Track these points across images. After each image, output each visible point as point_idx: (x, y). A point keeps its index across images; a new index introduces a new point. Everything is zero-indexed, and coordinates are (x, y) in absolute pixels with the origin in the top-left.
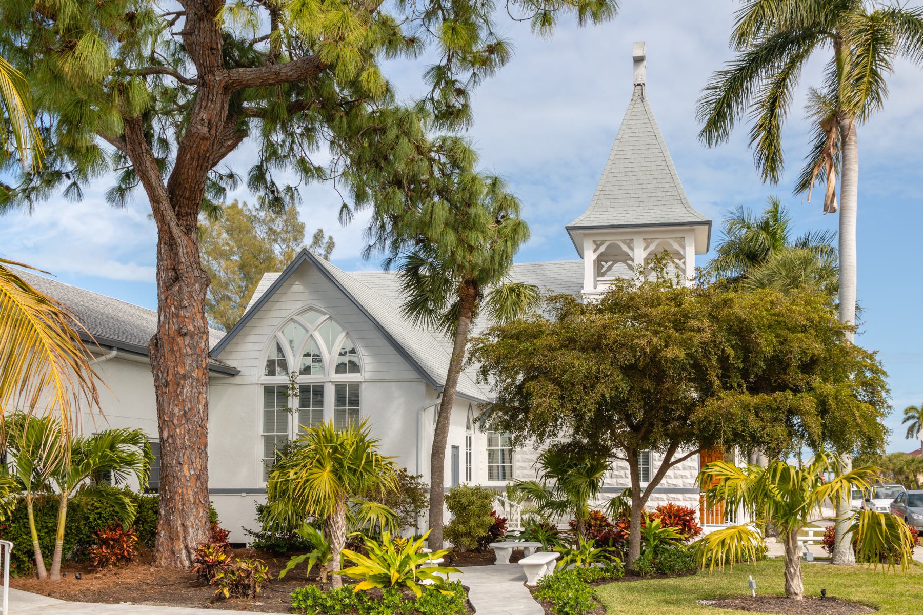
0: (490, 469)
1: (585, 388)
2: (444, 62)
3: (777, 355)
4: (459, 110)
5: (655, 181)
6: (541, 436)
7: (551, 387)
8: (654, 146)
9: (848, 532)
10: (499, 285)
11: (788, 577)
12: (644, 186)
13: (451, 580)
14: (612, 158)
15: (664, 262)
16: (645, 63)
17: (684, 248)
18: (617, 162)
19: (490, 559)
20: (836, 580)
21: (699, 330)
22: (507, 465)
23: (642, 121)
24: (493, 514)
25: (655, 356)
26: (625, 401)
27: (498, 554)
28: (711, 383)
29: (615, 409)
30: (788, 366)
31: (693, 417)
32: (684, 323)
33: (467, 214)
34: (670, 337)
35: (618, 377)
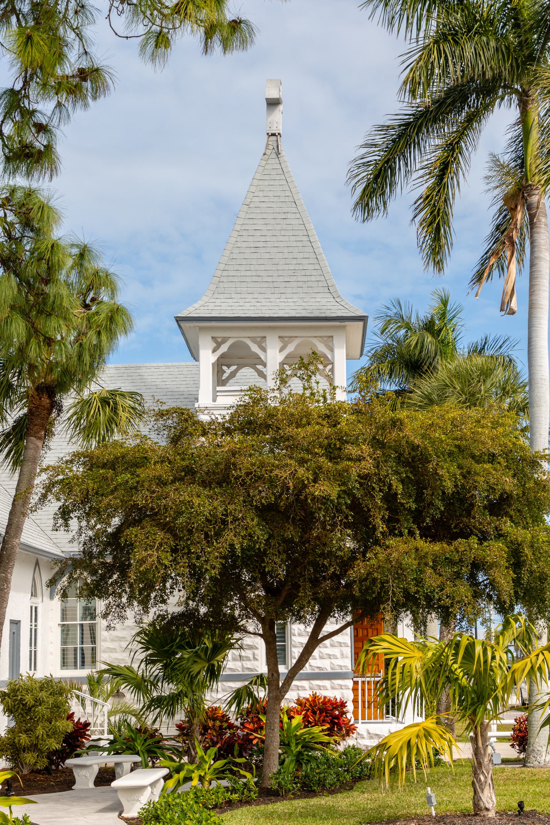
0: (64, 652)
1: (207, 536)
2: (18, 86)
3: (458, 493)
4: (40, 152)
5: (294, 261)
6: (145, 603)
7: (160, 535)
8: (293, 216)
9: (543, 726)
10: (86, 393)
11: (476, 788)
12: (280, 267)
13: (14, 815)
14: (238, 227)
15: (312, 368)
16: (281, 107)
17: (332, 350)
18: (245, 233)
19: (66, 782)
20: (532, 788)
21: (359, 459)
22: (88, 646)
23: (277, 183)
24: (70, 717)
25: (300, 492)
26: (261, 555)
27: (78, 774)
28: (374, 529)
29: (247, 566)
30: (472, 505)
31: (352, 574)
32: (340, 449)
33: (45, 296)
34: (320, 468)
35: (253, 522)
